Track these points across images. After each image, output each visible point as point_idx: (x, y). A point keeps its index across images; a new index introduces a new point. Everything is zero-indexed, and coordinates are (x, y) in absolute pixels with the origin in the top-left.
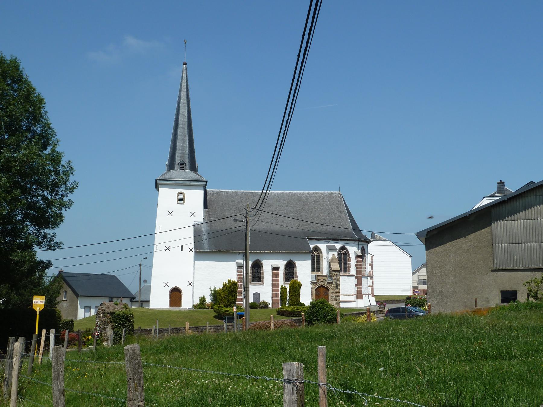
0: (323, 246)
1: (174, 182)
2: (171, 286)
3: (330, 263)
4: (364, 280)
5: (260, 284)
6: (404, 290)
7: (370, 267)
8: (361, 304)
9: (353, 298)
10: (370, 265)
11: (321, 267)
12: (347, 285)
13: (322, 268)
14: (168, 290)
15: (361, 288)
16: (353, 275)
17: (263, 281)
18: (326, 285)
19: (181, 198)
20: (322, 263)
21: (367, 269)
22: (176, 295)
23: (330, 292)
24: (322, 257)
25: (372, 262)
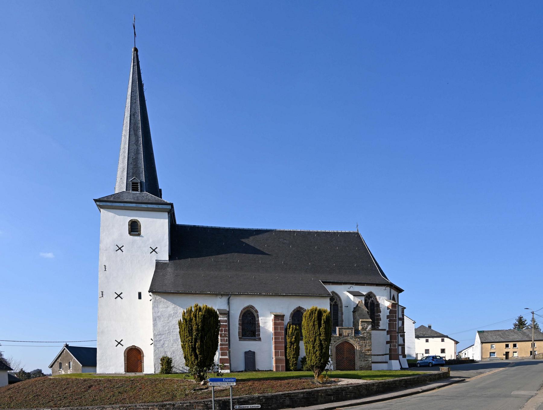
1: (122, 204)
2: (127, 344)
3: (354, 312)
5: (255, 340)
7: (400, 322)
11: (339, 319)
14: (416, 339)
16: (385, 330)
17: (259, 335)
19: (134, 228)
20: (342, 314)
22: (134, 357)
24: (341, 307)
25: (403, 315)
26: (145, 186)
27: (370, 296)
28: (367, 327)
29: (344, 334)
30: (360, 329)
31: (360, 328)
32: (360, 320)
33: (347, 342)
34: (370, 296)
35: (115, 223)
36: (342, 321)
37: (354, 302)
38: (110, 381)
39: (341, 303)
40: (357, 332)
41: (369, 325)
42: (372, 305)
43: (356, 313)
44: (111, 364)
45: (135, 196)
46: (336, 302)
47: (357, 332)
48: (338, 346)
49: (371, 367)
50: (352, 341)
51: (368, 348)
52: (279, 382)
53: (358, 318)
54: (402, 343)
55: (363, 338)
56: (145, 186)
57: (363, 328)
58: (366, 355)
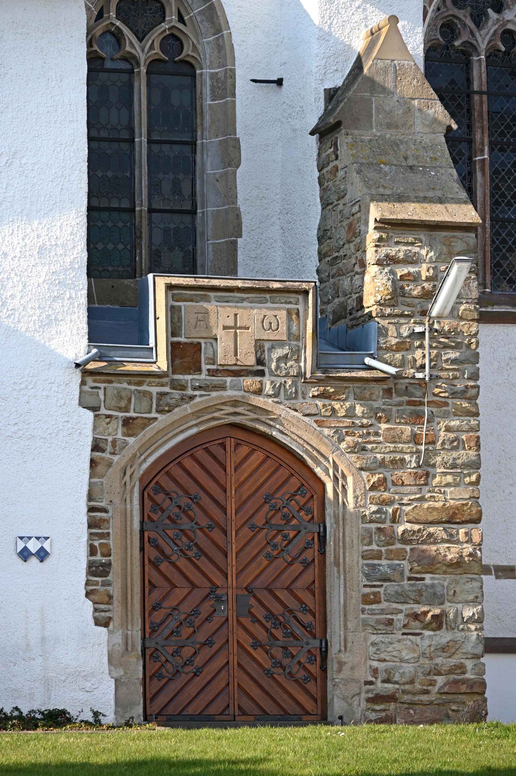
3: (326, 131)
11: (209, 209)
20: (231, 154)
24: (225, 86)
28: (437, 279)
29: (223, 352)
30: (370, 302)
31: (374, 286)
32: (375, 212)
33: (248, 435)
36: (232, 224)
37: (325, 37)
39: (224, 49)
40: (343, 327)
41: (446, 257)
43: (343, 140)
45: (314, 745)
46: (173, 41)
47: (343, 327)
48: (163, 466)
49: (479, 688)
50: (295, 426)
51: (454, 497)
53: (356, 188)
55: (403, 395)
57: (397, 294)
58: (431, 564)
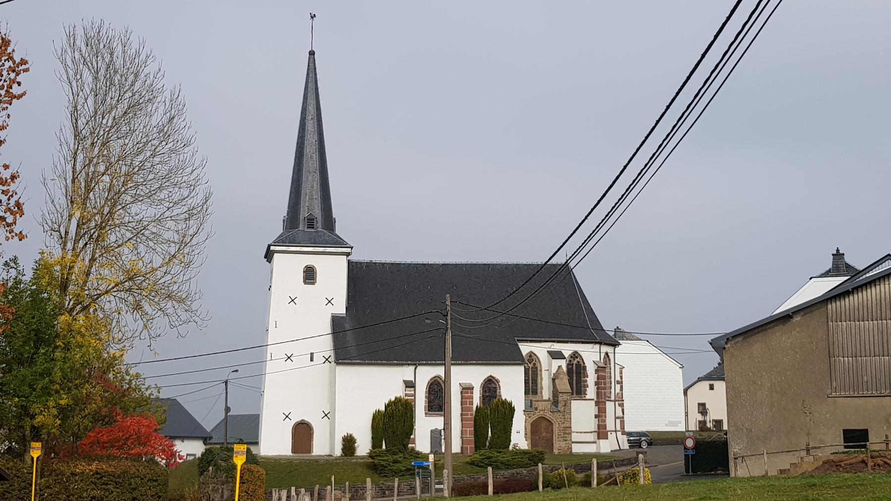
0: (541, 350)
2: (296, 419)
3: (554, 380)
4: (610, 406)
6: (671, 423)
7: (618, 386)
8: (606, 447)
9: (592, 437)
10: (618, 382)
12: (582, 413)
13: (542, 388)
14: (290, 424)
15: (605, 421)
18: (548, 415)
19: (310, 275)
20: (542, 379)
21: (613, 390)
22: (302, 433)
23: (556, 427)
24: (541, 371)
25: (621, 377)
26: (309, 221)
27: (575, 355)
34: (575, 355)
35: (289, 265)
38: (275, 465)
42: (576, 370)
44: (275, 442)
52: (532, 281)
54: (621, 415)
56: (309, 221)
